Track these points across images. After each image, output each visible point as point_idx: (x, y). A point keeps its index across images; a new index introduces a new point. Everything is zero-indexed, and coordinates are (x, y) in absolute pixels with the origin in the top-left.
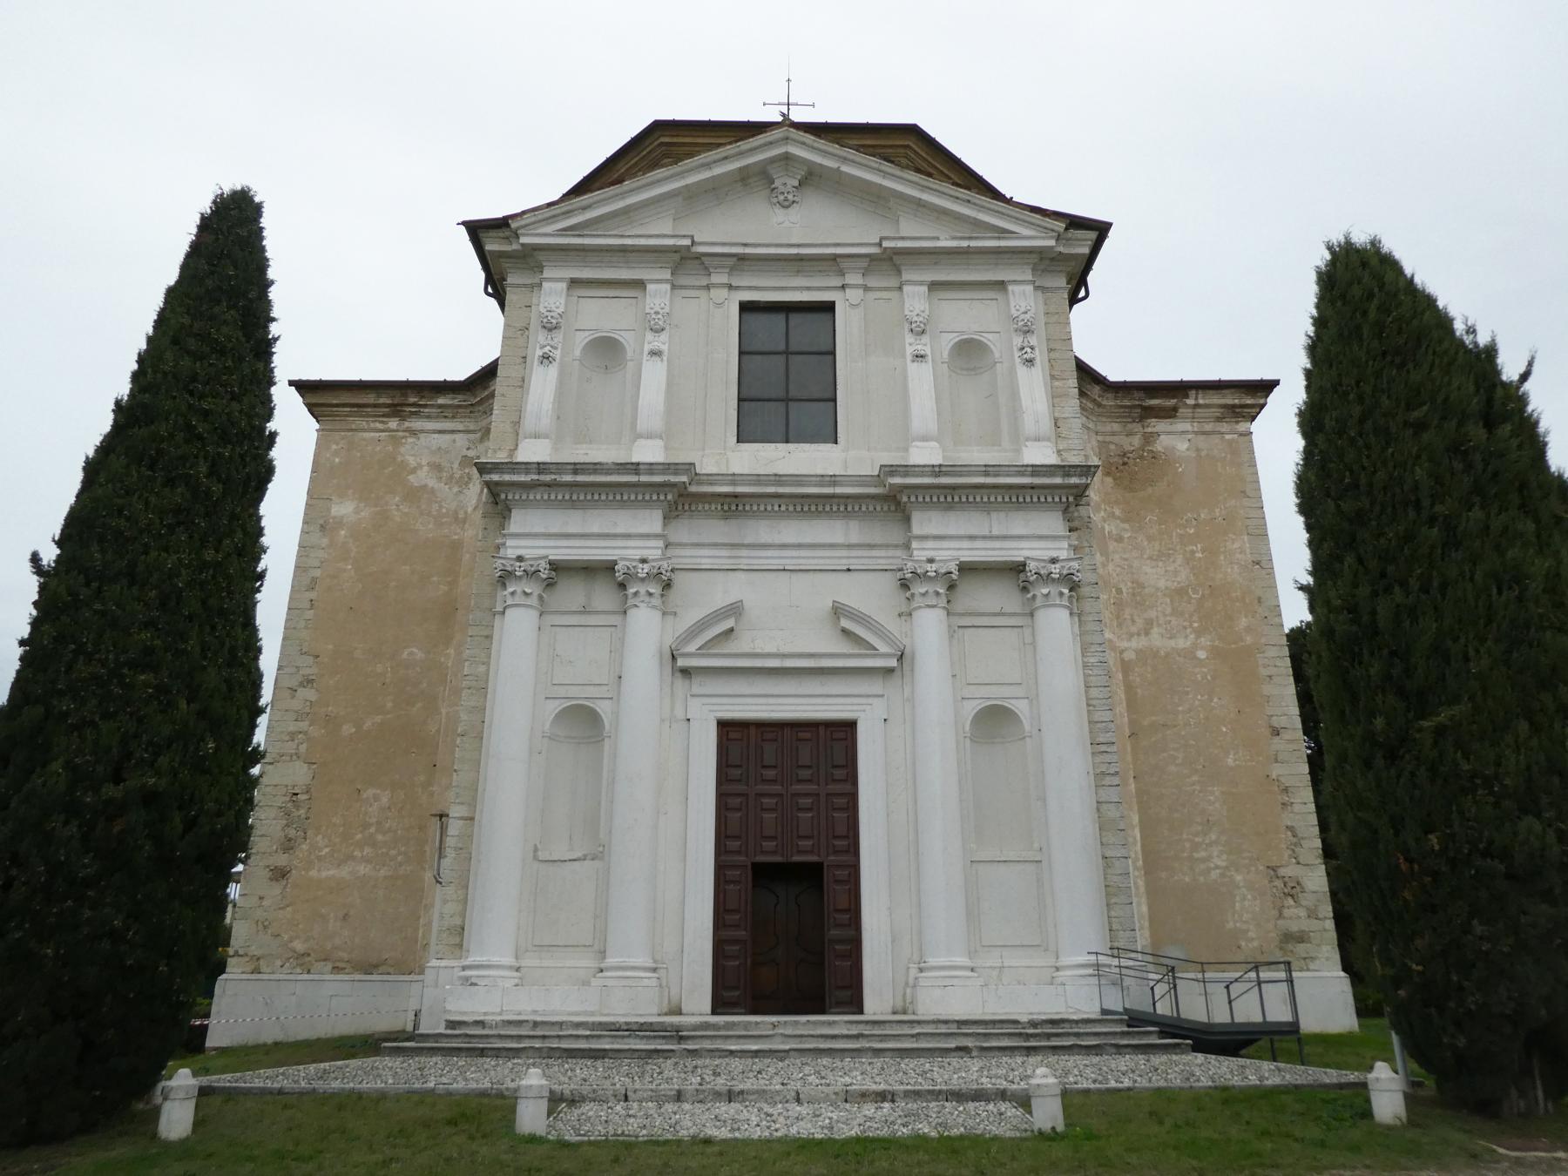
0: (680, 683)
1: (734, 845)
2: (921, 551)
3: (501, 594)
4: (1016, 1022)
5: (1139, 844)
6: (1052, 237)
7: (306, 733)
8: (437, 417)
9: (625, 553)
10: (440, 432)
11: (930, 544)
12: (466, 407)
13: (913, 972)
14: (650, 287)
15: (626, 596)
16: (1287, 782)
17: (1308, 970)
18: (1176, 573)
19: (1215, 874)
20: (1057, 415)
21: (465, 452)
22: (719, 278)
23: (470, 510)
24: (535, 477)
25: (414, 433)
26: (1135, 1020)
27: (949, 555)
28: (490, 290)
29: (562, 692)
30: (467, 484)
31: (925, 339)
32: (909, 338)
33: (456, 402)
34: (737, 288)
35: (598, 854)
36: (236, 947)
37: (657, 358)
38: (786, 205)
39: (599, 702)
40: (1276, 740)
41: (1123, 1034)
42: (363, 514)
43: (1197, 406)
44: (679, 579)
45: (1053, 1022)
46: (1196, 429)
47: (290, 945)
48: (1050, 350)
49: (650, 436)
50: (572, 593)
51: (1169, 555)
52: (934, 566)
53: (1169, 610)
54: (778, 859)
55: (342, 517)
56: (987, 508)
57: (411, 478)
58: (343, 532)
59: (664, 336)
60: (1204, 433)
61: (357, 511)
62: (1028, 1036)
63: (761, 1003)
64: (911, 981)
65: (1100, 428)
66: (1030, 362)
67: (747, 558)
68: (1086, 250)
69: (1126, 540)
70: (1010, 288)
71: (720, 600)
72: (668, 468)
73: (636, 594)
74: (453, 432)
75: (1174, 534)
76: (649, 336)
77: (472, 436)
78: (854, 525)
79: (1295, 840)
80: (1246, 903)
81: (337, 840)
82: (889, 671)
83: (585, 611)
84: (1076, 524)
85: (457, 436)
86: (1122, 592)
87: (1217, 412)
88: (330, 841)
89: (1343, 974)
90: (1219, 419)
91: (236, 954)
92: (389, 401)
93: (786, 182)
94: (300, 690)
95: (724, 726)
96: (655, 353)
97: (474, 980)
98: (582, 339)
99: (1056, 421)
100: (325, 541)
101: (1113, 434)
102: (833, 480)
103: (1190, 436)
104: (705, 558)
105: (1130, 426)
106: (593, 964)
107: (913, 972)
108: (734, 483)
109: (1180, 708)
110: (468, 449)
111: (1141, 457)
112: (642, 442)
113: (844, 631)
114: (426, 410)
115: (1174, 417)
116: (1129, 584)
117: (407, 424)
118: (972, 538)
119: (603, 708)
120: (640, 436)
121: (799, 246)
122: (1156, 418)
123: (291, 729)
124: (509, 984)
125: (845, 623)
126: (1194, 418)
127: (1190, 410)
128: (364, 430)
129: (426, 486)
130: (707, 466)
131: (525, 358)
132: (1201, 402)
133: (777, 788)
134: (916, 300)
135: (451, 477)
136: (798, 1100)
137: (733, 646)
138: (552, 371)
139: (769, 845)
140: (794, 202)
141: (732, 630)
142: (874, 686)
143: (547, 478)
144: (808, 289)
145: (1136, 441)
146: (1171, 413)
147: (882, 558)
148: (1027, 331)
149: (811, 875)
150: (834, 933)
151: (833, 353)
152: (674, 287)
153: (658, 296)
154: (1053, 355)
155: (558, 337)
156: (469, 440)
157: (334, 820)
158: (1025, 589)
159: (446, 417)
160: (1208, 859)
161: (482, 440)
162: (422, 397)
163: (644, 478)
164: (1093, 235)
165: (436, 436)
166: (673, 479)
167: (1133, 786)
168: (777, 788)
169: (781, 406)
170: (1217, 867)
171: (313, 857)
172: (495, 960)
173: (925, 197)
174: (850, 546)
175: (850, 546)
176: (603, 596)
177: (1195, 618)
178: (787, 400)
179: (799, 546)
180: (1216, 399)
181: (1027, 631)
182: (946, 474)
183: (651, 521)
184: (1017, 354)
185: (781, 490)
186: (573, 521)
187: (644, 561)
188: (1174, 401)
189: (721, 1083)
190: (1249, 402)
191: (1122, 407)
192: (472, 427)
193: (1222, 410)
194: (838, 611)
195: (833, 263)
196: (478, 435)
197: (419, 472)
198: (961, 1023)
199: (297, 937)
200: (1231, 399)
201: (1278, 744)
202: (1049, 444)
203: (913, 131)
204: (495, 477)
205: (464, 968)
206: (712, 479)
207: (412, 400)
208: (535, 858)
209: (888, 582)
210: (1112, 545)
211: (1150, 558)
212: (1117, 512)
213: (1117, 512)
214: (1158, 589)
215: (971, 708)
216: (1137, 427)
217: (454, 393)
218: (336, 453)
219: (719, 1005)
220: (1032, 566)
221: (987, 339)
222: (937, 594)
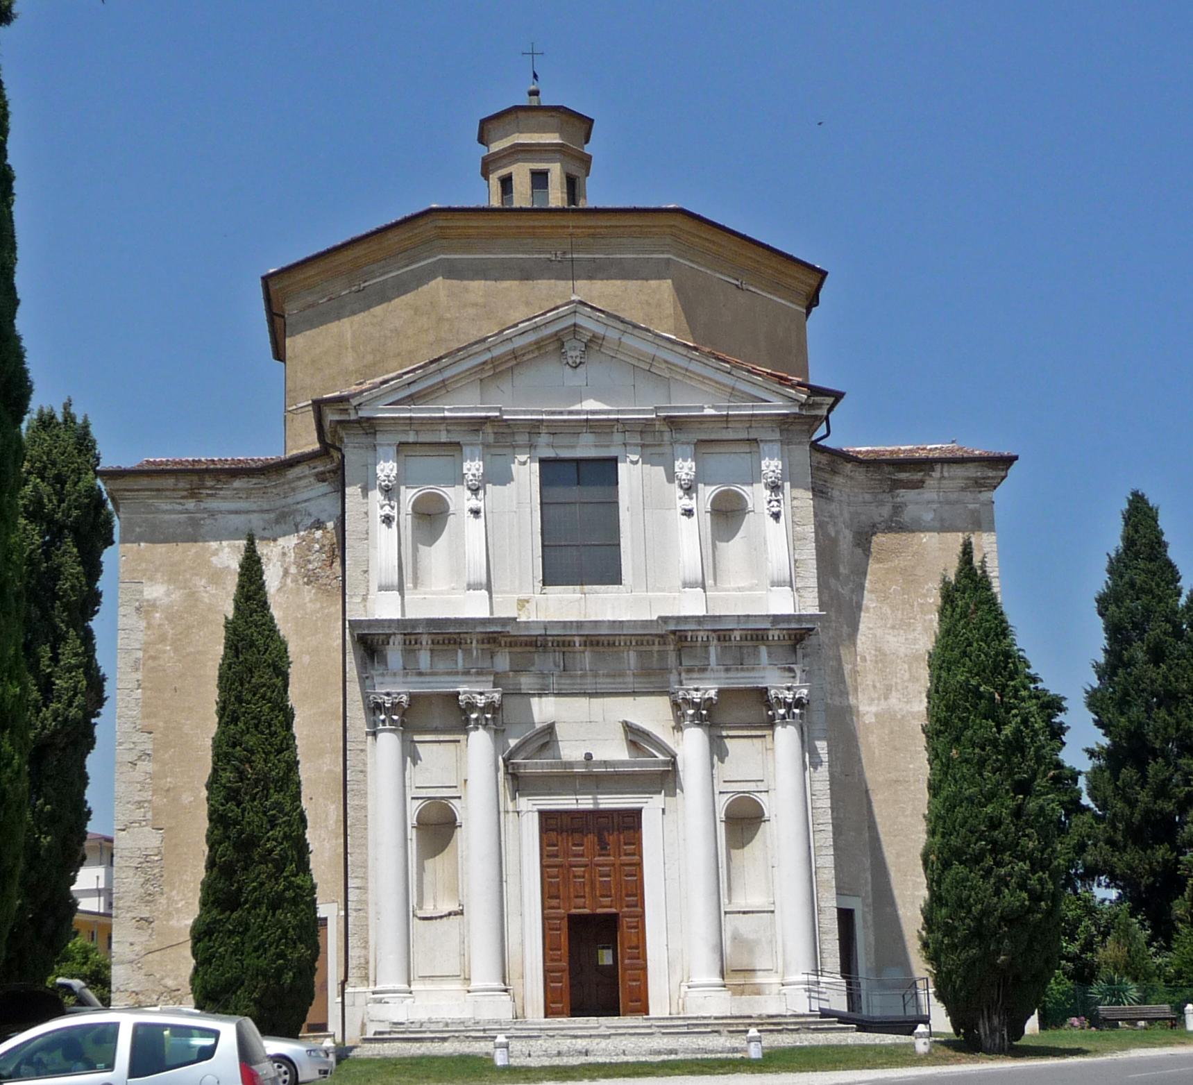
5: (870, 885)
6: (795, 406)
7: (149, 802)
8: (233, 498)
10: (237, 512)
12: (259, 489)
18: (915, 641)
20: (796, 557)
26: (825, 1014)
29: (424, 793)
36: (118, 985)
39: (452, 801)
42: (173, 596)
43: (942, 478)
46: (941, 499)
47: (163, 982)
51: (910, 625)
53: (907, 676)
54: (587, 911)
55: (155, 600)
57: (214, 559)
58: (158, 615)
61: (168, 594)
63: (577, 1010)
64: (682, 994)
69: (872, 610)
70: (762, 445)
74: (247, 512)
75: (916, 603)
77: (266, 516)
81: (190, 894)
86: (866, 660)
87: (961, 483)
88: (184, 895)
90: (963, 489)
94: (139, 763)
96: (476, 513)
97: (386, 1000)
103: (935, 506)
105: (880, 497)
109: (911, 766)
110: (264, 529)
114: (221, 492)
116: (873, 652)
117: (203, 505)
123: (137, 798)
128: (165, 512)
129: (228, 567)
131: (366, 513)
133: (584, 860)
136: (624, 1054)
140: (581, 363)
141: (548, 742)
146: (919, 485)
154: (795, 503)
156: (264, 520)
157: (185, 877)
159: (240, 498)
161: (277, 522)
162: (219, 481)
164: (830, 400)
165: (232, 516)
167: (867, 835)
171: (171, 909)
172: (390, 987)
180: (958, 471)
190: (990, 475)
192: (266, 507)
194: (629, 728)
196: (272, 516)
197: (220, 554)
199: (168, 976)
200: (973, 471)
211: (893, 627)
217: (248, 477)
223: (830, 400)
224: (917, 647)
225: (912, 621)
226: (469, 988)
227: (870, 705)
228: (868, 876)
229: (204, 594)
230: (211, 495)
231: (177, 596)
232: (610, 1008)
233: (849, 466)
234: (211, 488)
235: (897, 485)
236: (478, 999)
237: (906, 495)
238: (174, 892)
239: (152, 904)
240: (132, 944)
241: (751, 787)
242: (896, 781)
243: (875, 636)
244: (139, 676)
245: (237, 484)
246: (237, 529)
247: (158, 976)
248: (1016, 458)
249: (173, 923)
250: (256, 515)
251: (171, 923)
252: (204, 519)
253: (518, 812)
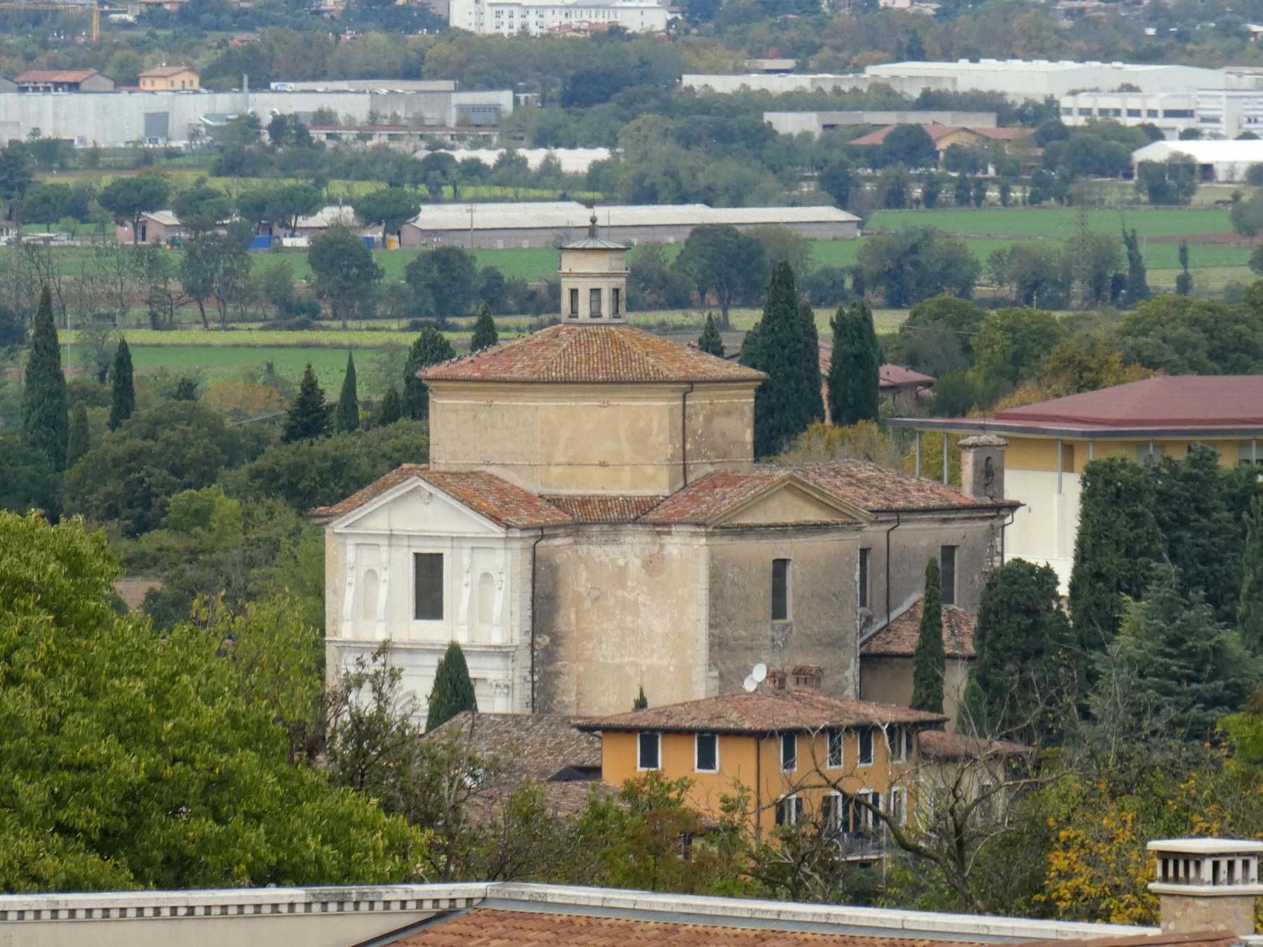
216: (657, 539)
235: (659, 533)
237: (666, 539)
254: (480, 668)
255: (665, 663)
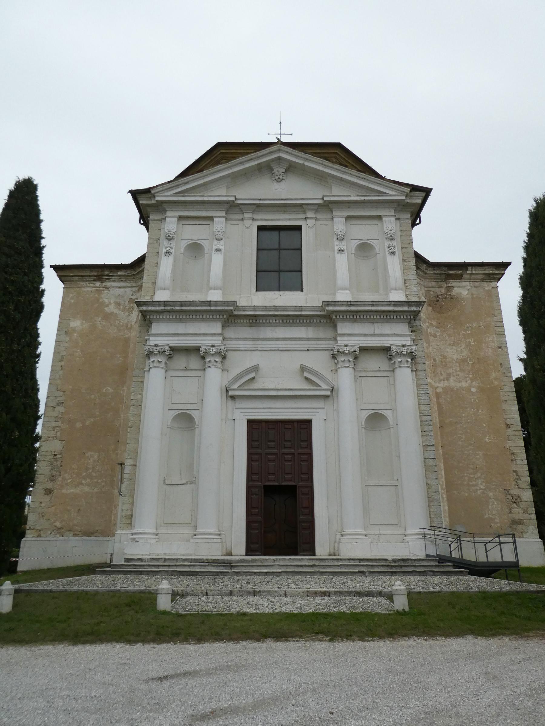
0: (230, 403)
1: (255, 477)
2: (342, 341)
3: (148, 362)
4: (386, 560)
6: (404, 195)
9: (204, 343)
11: (346, 338)
12: (131, 276)
13: (338, 536)
14: (216, 220)
15: (205, 362)
16: (513, 450)
17: (523, 537)
18: (462, 352)
19: (479, 492)
21: (131, 297)
22: (247, 215)
23: (133, 323)
24: (163, 308)
25: (107, 288)
26: (442, 559)
27: (355, 343)
28: (142, 222)
30: (132, 311)
31: (344, 242)
32: (336, 242)
33: (127, 274)
34: (256, 220)
35: (193, 481)
36: (30, 526)
37: (218, 252)
38: (279, 181)
40: (509, 430)
41: (436, 566)
43: (472, 274)
44: (229, 355)
45: (404, 560)
48: (403, 248)
49: (216, 289)
50: (180, 361)
51: (458, 344)
52: (348, 348)
53: (458, 369)
54: (276, 484)
56: (373, 321)
57: (106, 309)
58: (75, 335)
59: (222, 242)
60: (475, 287)
61: (82, 324)
62: (392, 567)
65: (426, 284)
66: (393, 253)
67: (261, 344)
68: (420, 201)
70: (384, 219)
71: (249, 364)
72: (224, 303)
73: (210, 361)
75: (461, 334)
76: (215, 242)
77: (134, 289)
78: (310, 329)
79: (517, 477)
80: (494, 506)
82: (327, 397)
83: (186, 370)
84: (414, 329)
85: (127, 290)
87: (481, 277)
88: (71, 476)
89: (539, 540)
90: (482, 280)
91: (30, 529)
92: (96, 274)
93: (279, 170)
95: (251, 423)
97: (137, 540)
98: (184, 244)
99: (405, 280)
100: (67, 339)
101: (432, 287)
102: (301, 308)
103: (468, 288)
104: (241, 344)
105: (440, 283)
106: (192, 532)
107: (338, 536)
108: (255, 310)
110: (132, 295)
111: (446, 298)
112: (212, 291)
113: (306, 378)
114: (113, 278)
115: (461, 279)
116: (440, 357)
117: (104, 284)
118: (365, 335)
119: (195, 414)
120: (211, 289)
121: (285, 200)
122: (452, 279)
123: (54, 425)
124: (153, 541)
125: (306, 374)
126: (470, 280)
127: (468, 276)
128: (85, 287)
130: (242, 302)
131: (158, 253)
132: (474, 272)
134: (339, 225)
135: (125, 308)
136: (286, 595)
137: (255, 385)
138: (171, 259)
139: (271, 477)
140: (283, 179)
141: (254, 378)
142: (320, 404)
143: (169, 308)
144: (289, 219)
145: (443, 290)
146: (459, 277)
147: (324, 344)
148: (392, 239)
149: (291, 491)
150: (259, 518)
151: (300, 249)
152: (227, 219)
153: (219, 224)
154: (404, 250)
155: (173, 243)
158: (390, 359)
159: (122, 281)
160: (476, 485)
163: (213, 308)
164: (423, 194)
165: (117, 289)
166: (226, 308)
167: (441, 450)
168: (275, 451)
169: (276, 274)
170: (481, 489)
172: (147, 530)
173: (344, 176)
174: (308, 339)
175: (308, 339)
176: (194, 363)
177: (471, 373)
178: (279, 271)
179: (285, 339)
180: (481, 271)
181: (391, 379)
182: (353, 305)
183: (216, 328)
184: (387, 250)
185: (276, 313)
186: (180, 328)
187: (213, 346)
188: (460, 272)
189: (250, 587)
190: (497, 272)
191: (436, 274)
193: (483, 276)
194: (303, 369)
195: (300, 207)
196: (137, 289)
197: (110, 306)
198: (360, 560)
200: (488, 271)
201: (509, 432)
202: (401, 291)
203: (339, 146)
204: (145, 308)
205: (132, 534)
206: (244, 308)
207: (106, 273)
208: (164, 483)
209: (327, 355)
210: (431, 339)
211: (450, 345)
212: (434, 323)
213: (434, 323)
214: (453, 359)
215: (365, 414)
216: (444, 284)
218: (72, 298)
219: (249, 551)
220: (394, 348)
221: (374, 243)
222: (349, 361)
223: (423, 194)
224: (463, 355)
225: (460, 342)
226: (196, 533)
227: (439, 383)
228: (443, 473)
229: (99, 325)
230: (108, 279)
231: (86, 326)
232: (292, 550)
233: (425, 265)
234: (108, 275)
235: (449, 277)
236: (199, 541)
238: (66, 475)
239: (54, 481)
240: (41, 503)
241: (381, 406)
242: (456, 423)
243: (440, 349)
244: (62, 363)
245: (120, 273)
246: (119, 295)
247: (52, 520)
248: (509, 263)
249: (64, 491)
250: (129, 289)
251: (63, 491)
252: (104, 290)
253: (234, 419)
254: (253, 344)
255: (464, 384)
